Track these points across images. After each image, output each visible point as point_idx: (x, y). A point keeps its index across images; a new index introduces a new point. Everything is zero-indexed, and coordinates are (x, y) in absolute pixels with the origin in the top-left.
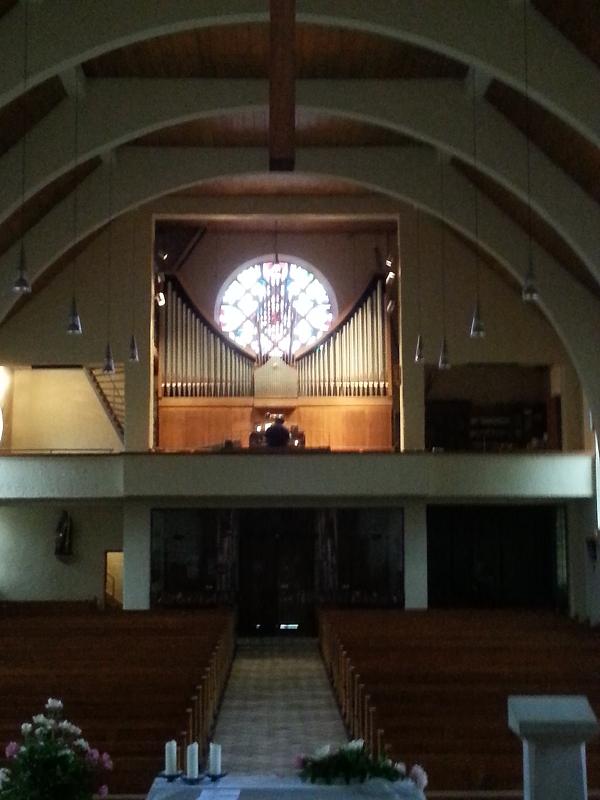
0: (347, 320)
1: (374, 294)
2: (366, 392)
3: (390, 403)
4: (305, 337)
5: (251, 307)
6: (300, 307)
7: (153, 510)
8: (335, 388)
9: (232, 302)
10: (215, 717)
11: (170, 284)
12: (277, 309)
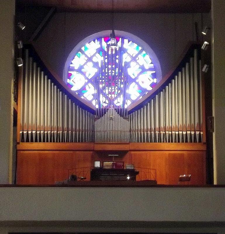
0: (168, 82)
1: (191, 59)
2: (185, 139)
3: (204, 148)
4: (134, 93)
5: (91, 71)
6: (133, 71)
7: (21, 142)
8: (160, 134)
9: (76, 68)
10: (16, 99)
11: (27, 51)
12: (113, 75)
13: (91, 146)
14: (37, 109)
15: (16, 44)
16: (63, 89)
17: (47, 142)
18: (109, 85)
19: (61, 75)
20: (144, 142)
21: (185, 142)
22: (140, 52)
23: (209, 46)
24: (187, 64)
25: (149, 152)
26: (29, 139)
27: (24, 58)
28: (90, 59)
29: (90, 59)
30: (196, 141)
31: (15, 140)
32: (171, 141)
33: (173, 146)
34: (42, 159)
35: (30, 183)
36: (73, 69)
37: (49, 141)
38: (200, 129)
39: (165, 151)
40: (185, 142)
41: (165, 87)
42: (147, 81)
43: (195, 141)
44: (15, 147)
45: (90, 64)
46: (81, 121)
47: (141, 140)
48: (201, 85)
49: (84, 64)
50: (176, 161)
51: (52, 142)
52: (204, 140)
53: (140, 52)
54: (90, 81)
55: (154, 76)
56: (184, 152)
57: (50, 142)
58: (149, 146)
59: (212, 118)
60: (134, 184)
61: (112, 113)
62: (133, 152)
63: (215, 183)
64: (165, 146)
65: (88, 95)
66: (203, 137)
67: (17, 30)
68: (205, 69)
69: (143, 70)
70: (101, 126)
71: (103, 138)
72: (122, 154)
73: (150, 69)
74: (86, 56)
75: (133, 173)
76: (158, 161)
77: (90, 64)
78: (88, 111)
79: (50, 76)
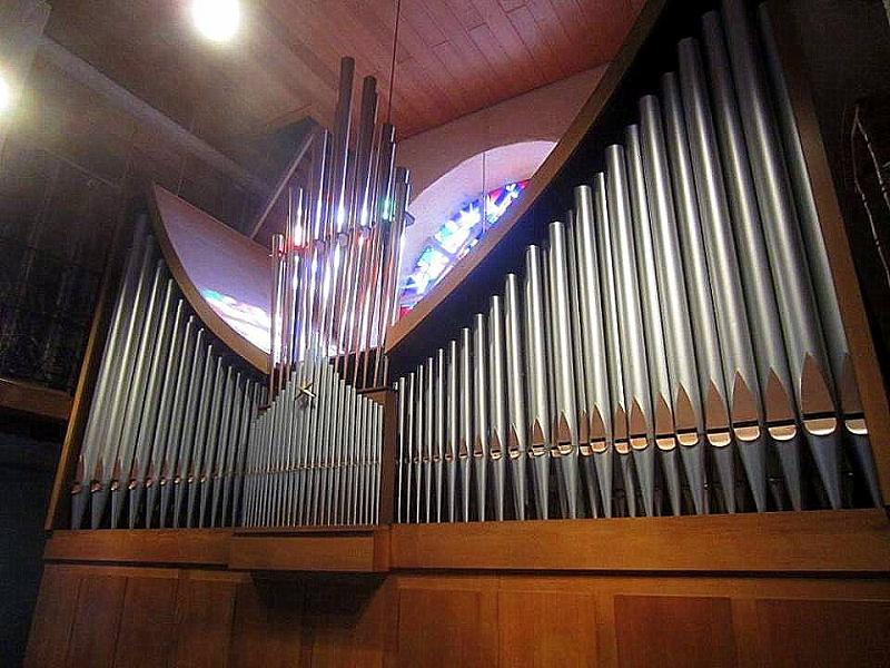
1: (709, 19)
2: (722, 487)
17: (192, 527)
20: (532, 512)
21: (677, 511)
24: (686, 46)
25: (493, 581)
30: (718, 507)
33: (640, 541)
37: (114, 522)
38: (836, 394)
39: (591, 581)
40: (677, 511)
41: (573, 192)
43: (814, 498)
48: (775, 57)
51: (109, 527)
56: (733, 590)
57: (119, 527)
58: (497, 541)
62: (404, 583)
64: (581, 540)
66: (877, 477)
71: (312, 511)
74: (445, 253)
78: (379, 404)
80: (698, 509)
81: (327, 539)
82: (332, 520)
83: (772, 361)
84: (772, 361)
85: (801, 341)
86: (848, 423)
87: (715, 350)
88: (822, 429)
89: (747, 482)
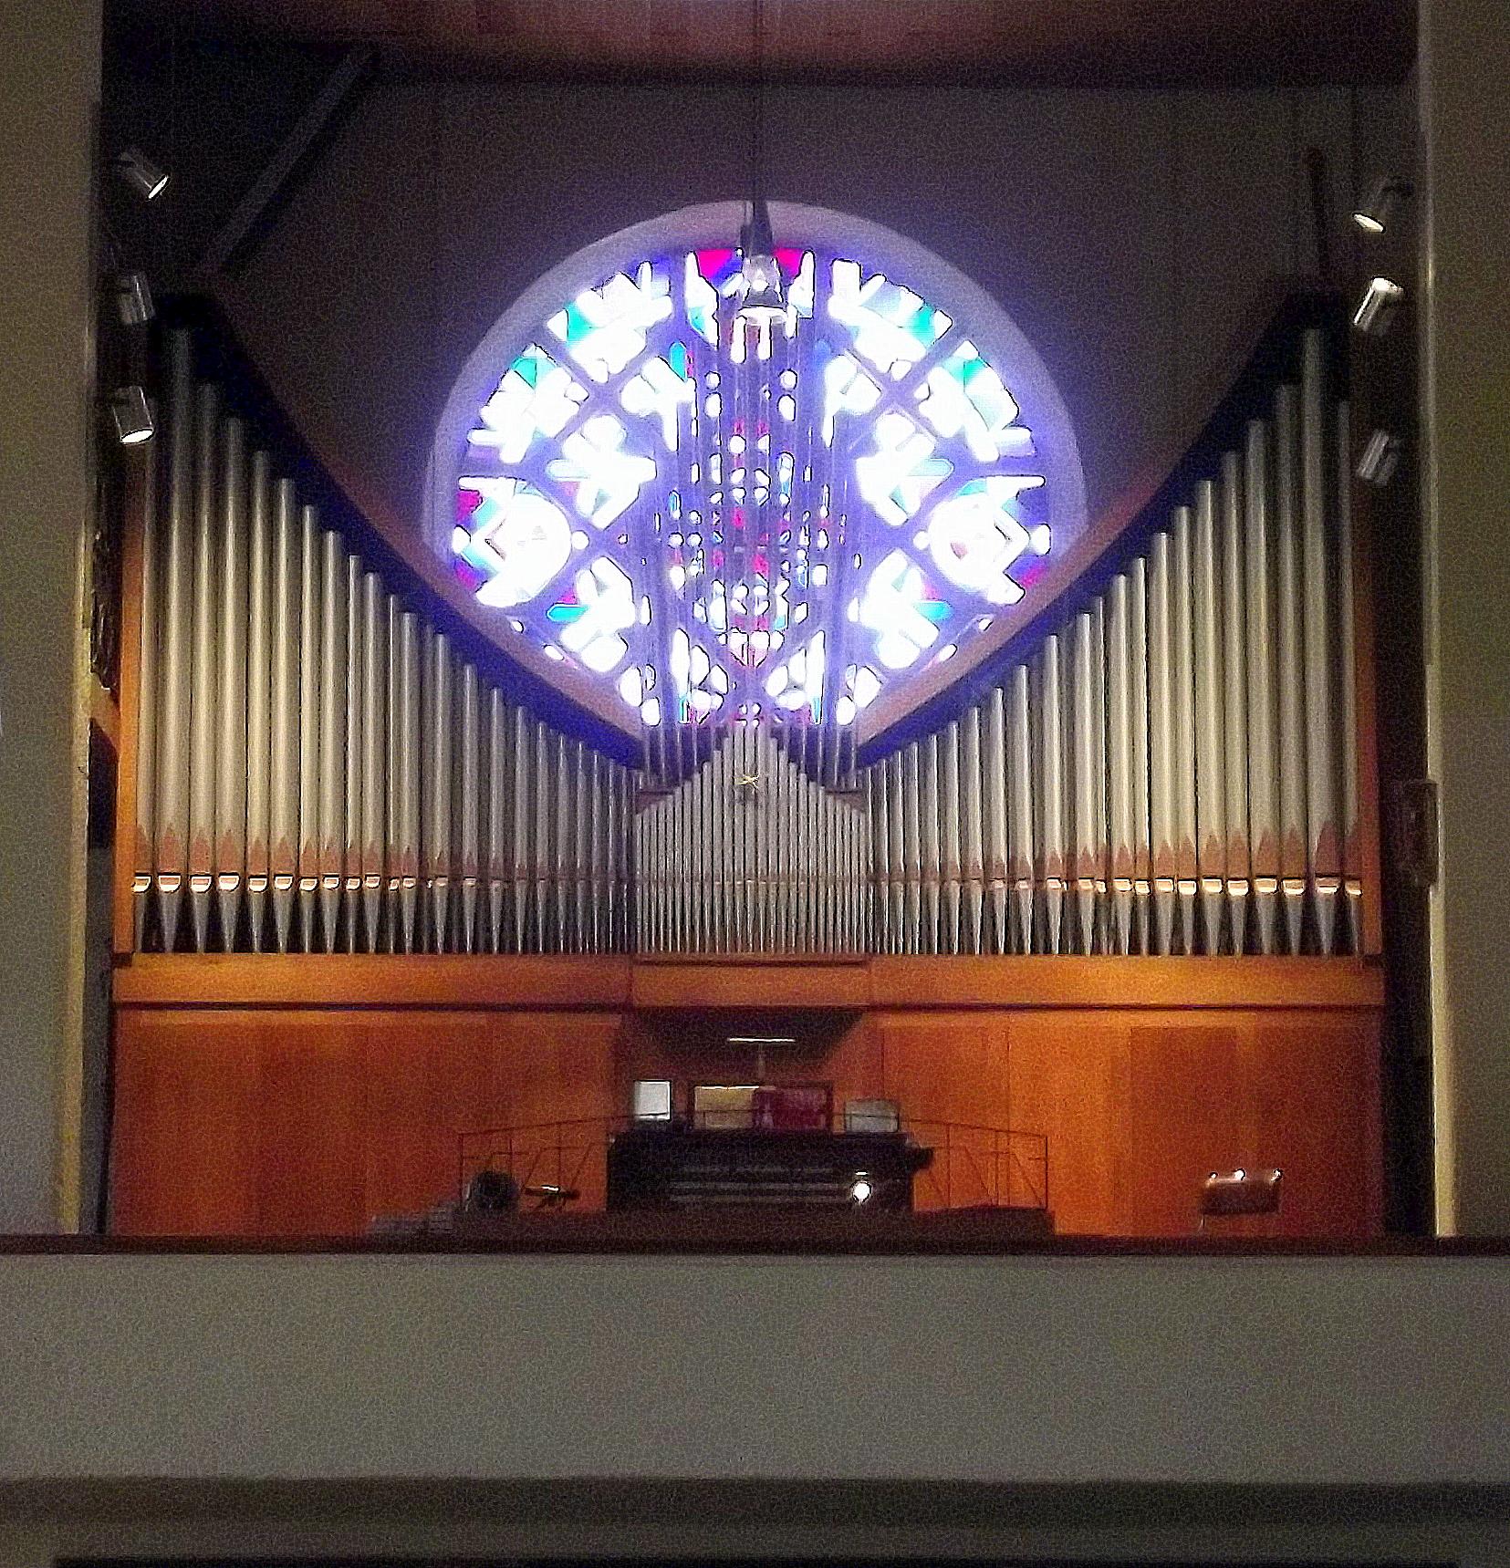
1: (1230, 462)
2: (1242, 935)
3: (1368, 990)
4: (900, 625)
5: (612, 477)
6: (889, 476)
8: (1071, 901)
9: (512, 454)
10: (108, 666)
12: (754, 500)
13: (612, 976)
14: (250, 729)
15: (107, 291)
16: (426, 599)
18: (730, 568)
19: (408, 503)
22: (943, 348)
23: (1403, 310)
25: (999, 1017)
26: (195, 930)
27: (159, 388)
28: (602, 398)
29: (602, 398)
31: (100, 935)
32: (1145, 942)
33: (1160, 978)
34: (280, 1065)
35: (203, 1226)
36: (488, 465)
37: (330, 944)
42: (986, 545)
43: (1309, 944)
44: (100, 984)
45: (606, 429)
46: (542, 814)
47: (941, 939)
49: (566, 431)
50: (1180, 1080)
52: (1369, 935)
53: (943, 348)
54: (602, 542)
55: (1034, 508)
59: (1422, 793)
60: (899, 1233)
61: (752, 759)
62: (890, 1022)
63: (1444, 1225)
65: (594, 636)
67: (115, 199)
68: (1373, 460)
69: (961, 467)
70: (677, 844)
72: (819, 1029)
73: (1009, 464)
75: (895, 1160)
76: (1057, 1080)
77: (606, 429)
79: (337, 514)
80: (1266, 950)
81: (253, 1000)
82: (674, 946)
83: (256, 830)
84: (1238, 822)
85: (1320, 812)
86: (1347, 885)
87: (289, 805)
88: (1265, 888)
89: (1230, 932)
